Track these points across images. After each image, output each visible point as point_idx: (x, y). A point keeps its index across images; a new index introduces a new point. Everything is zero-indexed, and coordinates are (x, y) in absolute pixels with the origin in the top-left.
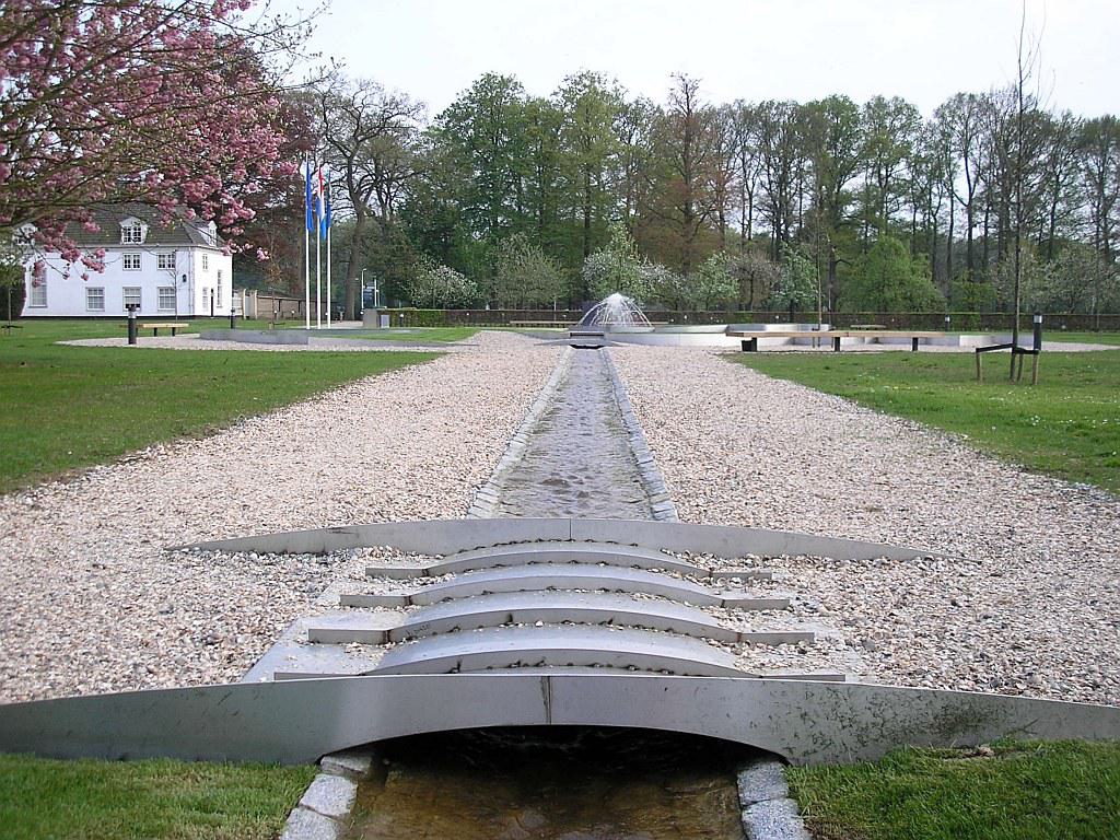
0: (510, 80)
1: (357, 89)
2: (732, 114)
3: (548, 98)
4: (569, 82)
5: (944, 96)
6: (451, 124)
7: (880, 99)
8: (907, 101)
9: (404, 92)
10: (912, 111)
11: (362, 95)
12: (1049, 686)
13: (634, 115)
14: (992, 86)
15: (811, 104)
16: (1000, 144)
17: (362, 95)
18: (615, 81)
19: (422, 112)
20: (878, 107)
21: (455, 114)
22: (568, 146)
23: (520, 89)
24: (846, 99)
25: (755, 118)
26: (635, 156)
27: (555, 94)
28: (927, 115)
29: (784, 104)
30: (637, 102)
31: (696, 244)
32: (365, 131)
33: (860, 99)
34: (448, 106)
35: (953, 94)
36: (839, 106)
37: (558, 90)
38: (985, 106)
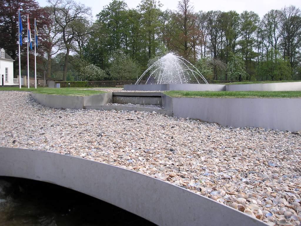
0: (122, 2)
1: (66, 3)
2: (198, 16)
3: (136, 8)
4: (143, 3)
5: (267, 11)
6: (102, 18)
7: (246, 12)
8: (255, 13)
9: (83, 4)
10: (257, 16)
11: (68, 5)
12: (213, 90)
13: (165, 16)
14: (285, 6)
15: (231, 12)
16: (286, 27)
17: (68, 5)
18: (159, 2)
19: (89, 11)
20: (245, 15)
21: (103, 15)
22: (6, 44)
23: (126, 6)
24: (235, 12)
25: (207, 17)
26: (164, 29)
27: (138, 7)
28: (261, 17)
29: (216, 12)
30: (166, 11)
31: (230, 85)
32: (68, 19)
33: (240, 12)
34: (101, 11)
35: (270, 10)
36: (233, 14)
37: (139, 5)
38: (281, 14)
